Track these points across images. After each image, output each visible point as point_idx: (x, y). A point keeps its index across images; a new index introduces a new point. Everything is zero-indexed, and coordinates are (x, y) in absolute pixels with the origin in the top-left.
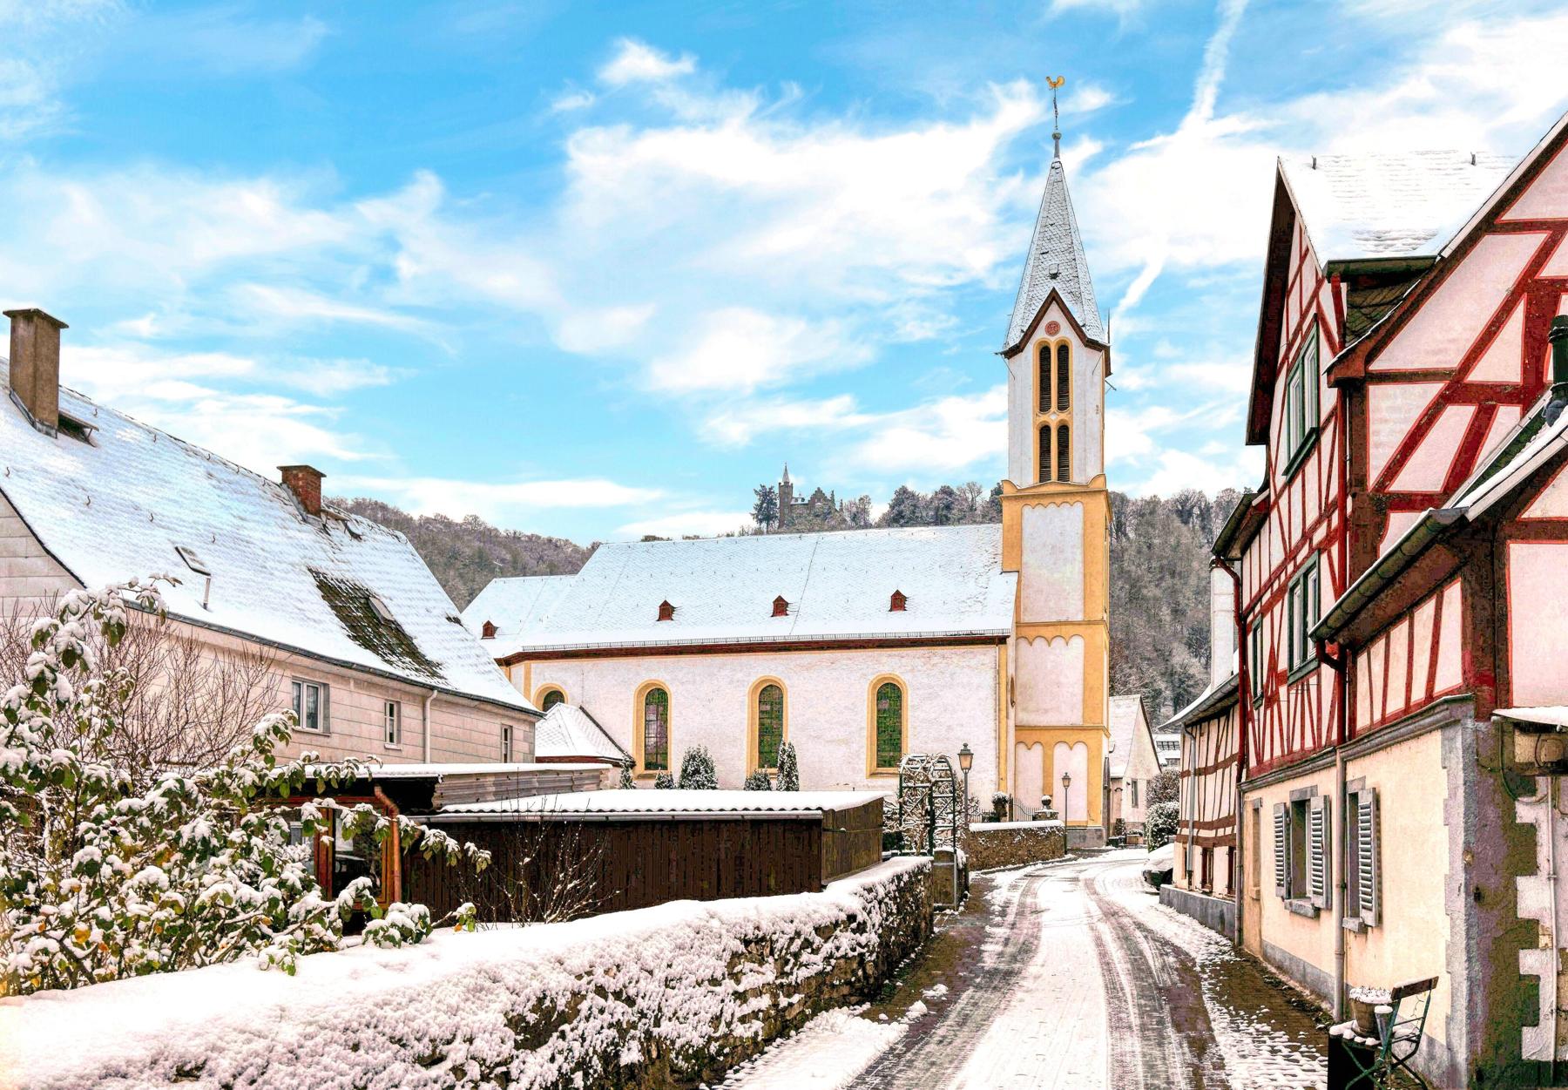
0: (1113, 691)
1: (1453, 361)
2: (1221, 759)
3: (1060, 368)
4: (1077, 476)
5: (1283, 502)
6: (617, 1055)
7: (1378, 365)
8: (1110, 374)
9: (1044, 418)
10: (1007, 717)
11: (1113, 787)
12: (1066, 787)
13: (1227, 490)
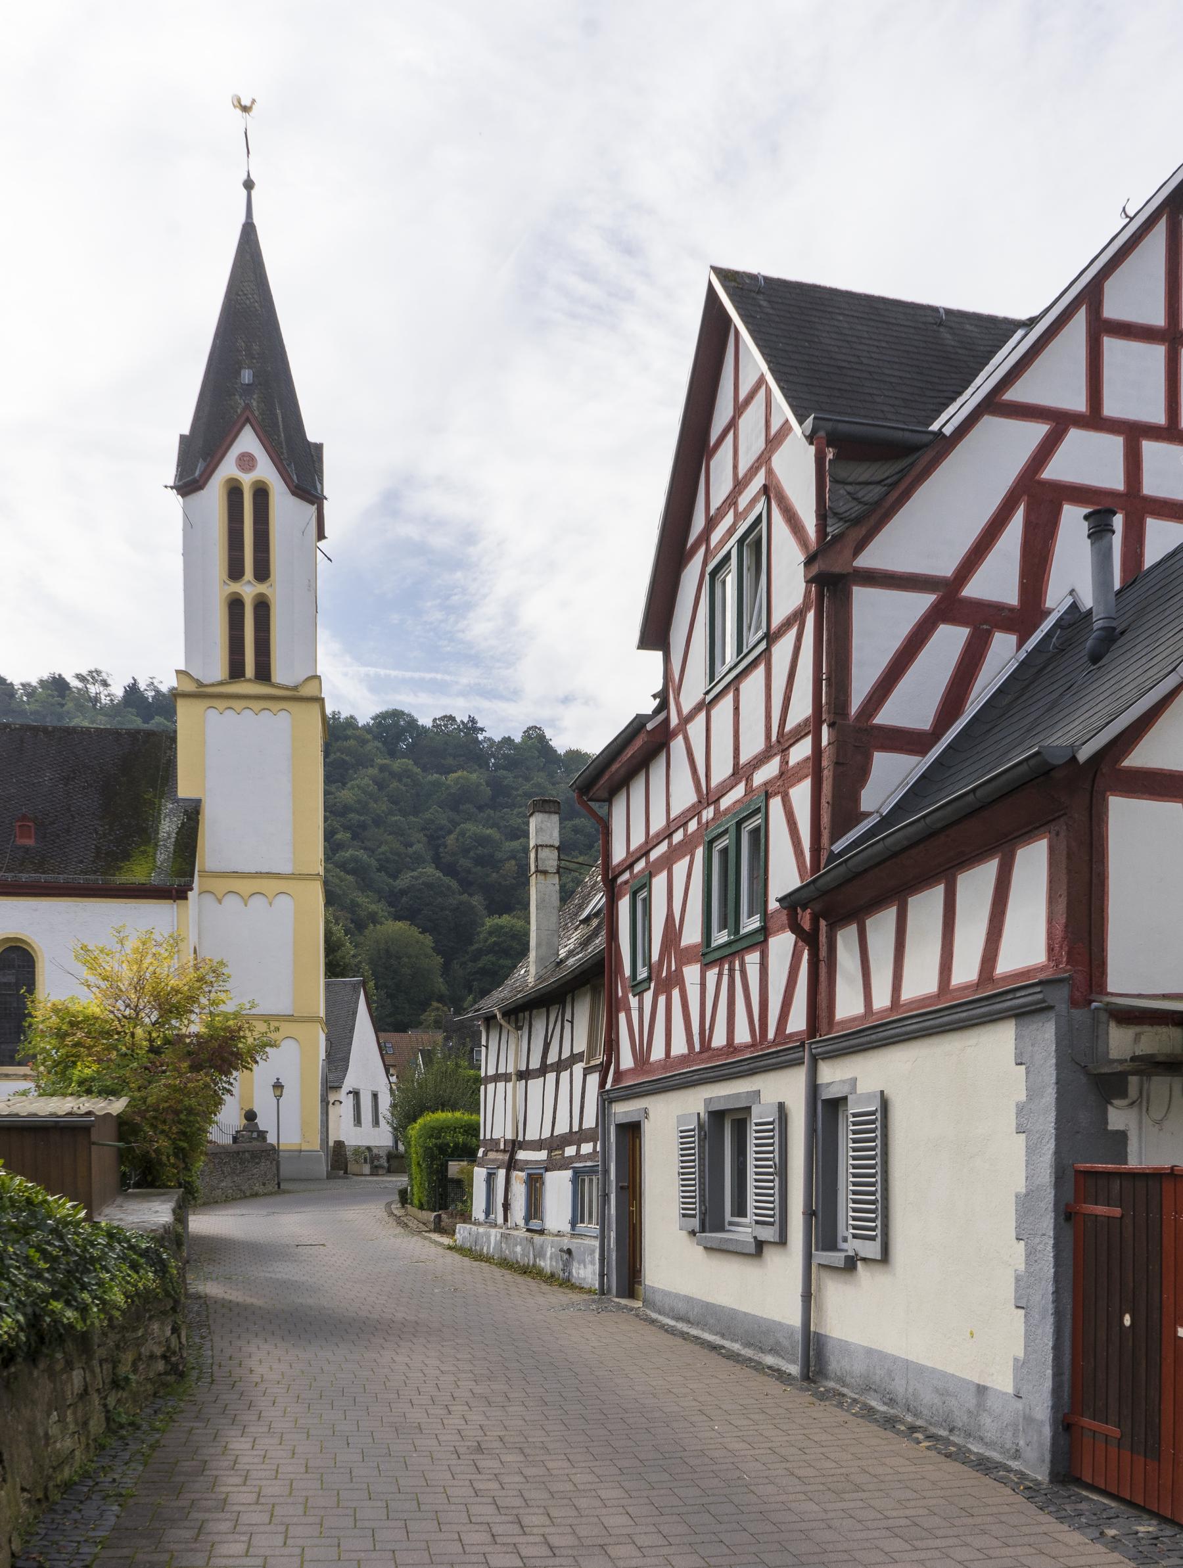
1: (946, 568)
2: (552, 1058)
3: (241, 521)
4: (282, 673)
5: (696, 729)
6: (171, 1370)
7: (868, 559)
9: (235, 587)
11: (332, 1098)
12: (278, 1097)
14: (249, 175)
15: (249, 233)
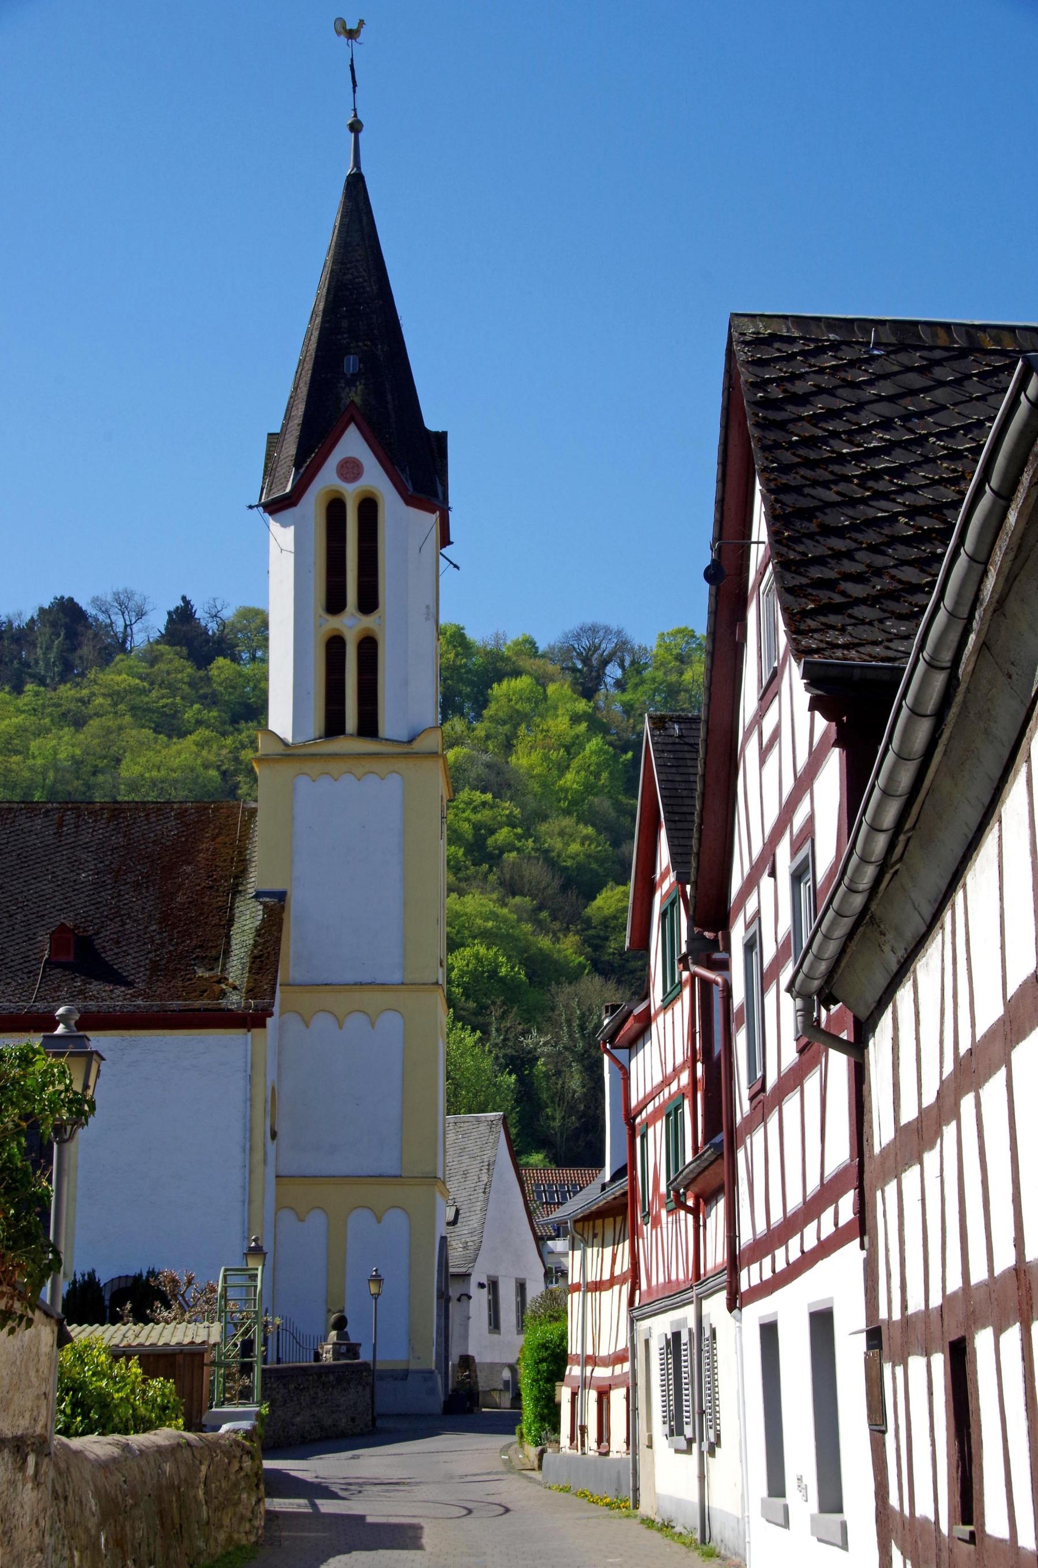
0: (453, 1108)
8: (450, 543)
10: (265, 1161)
11: (454, 1291)
13: (680, 631)
14: (355, 116)
15: (356, 186)
